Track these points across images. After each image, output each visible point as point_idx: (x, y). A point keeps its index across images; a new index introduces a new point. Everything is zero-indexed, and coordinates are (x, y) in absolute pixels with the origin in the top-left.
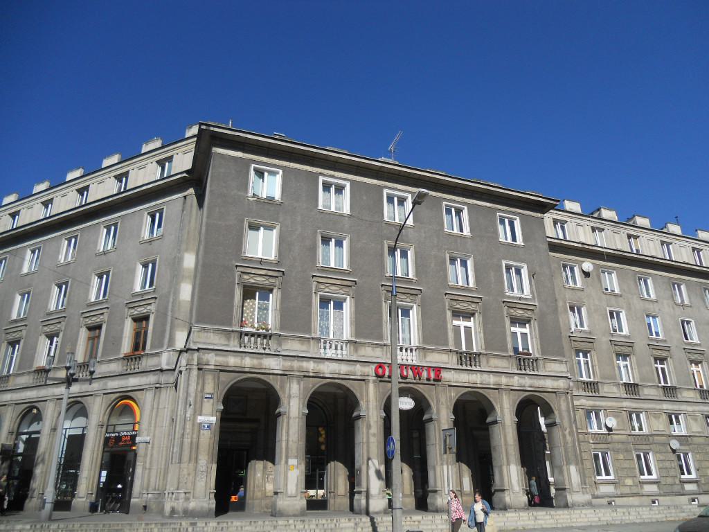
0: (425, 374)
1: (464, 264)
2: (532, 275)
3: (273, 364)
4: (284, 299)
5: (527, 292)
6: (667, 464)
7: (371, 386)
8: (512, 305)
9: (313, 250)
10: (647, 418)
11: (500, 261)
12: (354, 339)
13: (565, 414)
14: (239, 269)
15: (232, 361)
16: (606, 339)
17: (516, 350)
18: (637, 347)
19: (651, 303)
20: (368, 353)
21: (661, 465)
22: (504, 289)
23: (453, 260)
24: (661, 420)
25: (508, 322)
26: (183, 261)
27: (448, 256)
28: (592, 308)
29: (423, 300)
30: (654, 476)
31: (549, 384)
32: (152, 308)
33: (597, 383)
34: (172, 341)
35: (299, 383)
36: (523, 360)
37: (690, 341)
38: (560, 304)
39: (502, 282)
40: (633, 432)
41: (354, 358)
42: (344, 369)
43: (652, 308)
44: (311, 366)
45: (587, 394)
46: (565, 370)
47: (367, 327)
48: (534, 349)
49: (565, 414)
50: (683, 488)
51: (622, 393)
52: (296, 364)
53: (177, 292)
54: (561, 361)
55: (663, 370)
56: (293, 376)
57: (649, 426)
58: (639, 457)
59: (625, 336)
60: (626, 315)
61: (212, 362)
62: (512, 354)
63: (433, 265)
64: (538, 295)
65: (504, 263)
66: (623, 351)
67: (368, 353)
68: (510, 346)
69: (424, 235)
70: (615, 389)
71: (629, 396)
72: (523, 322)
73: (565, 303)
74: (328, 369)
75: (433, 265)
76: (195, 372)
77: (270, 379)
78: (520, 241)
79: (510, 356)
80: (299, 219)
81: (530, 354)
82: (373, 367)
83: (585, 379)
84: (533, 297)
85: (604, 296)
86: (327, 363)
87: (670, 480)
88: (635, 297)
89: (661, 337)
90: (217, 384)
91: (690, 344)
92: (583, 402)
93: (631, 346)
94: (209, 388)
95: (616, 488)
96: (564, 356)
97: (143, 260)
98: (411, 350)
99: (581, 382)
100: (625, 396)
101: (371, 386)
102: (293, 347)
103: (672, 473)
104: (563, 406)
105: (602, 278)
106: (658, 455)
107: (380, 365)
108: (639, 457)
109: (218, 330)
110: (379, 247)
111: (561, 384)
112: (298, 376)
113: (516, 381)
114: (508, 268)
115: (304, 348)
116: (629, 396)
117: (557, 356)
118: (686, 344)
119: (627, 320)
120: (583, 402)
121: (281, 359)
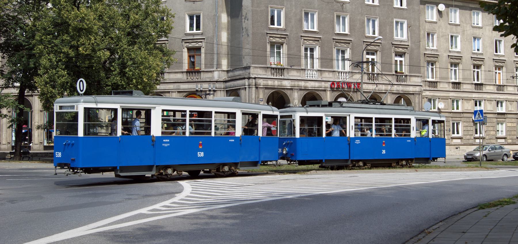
0: (353, 86)
1: (374, 22)
2: (409, 27)
3: (287, 84)
4: (289, 49)
5: (405, 37)
6: (469, 128)
7: (328, 93)
8: (397, 46)
9: (301, 21)
10: (462, 103)
11: (393, 19)
12: (320, 69)
13: (417, 105)
14: (268, 35)
15: (270, 83)
16: (446, 55)
17: (396, 72)
18: (464, 60)
19: (478, 29)
20: (328, 76)
21: (465, 129)
22: (393, 36)
23: (369, 20)
24: (470, 103)
25: (394, 55)
26: (221, 18)
27: (366, 18)
28: (441, 34)
29: (352, 46)
30: (460, 135)
31: (411, 89)
32: (203, 44)
33: (437, 82)
34: (219, 65)
35: (298, 93)
36: (399, 75)
37: (498, 53)
38: (422, 32)
39: (393, 33)
40: (453, 111)
41: (320, 79)
42: (317, 84)
43: (477, 32)
44: (302, 84)
45: (431, 89)
46: (420, 81)
47: (327, 62)
48: (405, 70)
49: (417, 105)
50: (475, 141)
51: (450, 87)
52: (296, 83)
53: (219, 37)
54: (418, 76)
55: (478, 72)
56: (295, 89)
57: (463, 107)
58: (453, 124)
59: (458, 52)
60: (461, 38)
61: (262, 84)
62: (394, 73)
63: (358, 25)
64: (411, 39)
65: (395, 20)
66: (455, 62)
67: (328, 76)
68: (394, 70)
69: (354, 7)
70: (446, 85)
71: (454, 90)
72: (401, 55)
73: (425, 32)
74: (310, 85)
75: (358, 25)
76: (254, 89)
77: (286, 92)
78: (404, 6)
79: (393, 75)
80: (294, 3)
81: (403, 73)
82: (330, 83)
83: (430, 79)
84: (408, 40)
85: (449, 26)
86: (309, 82)
87: (468, 137)
88: (468, 25)
89: (480, 52)
90: (264, 95)
91: (498, 56)
92: (427, 93)
93: (460, 58)
94: (261, 96)
95: (461, 141)
96: (420, 73)
97: (191, 13)
98: (346, 73)
99: (428, 81)
100: (452, 90)
101: (328, 93)
102: (294, 74)
103: (470, 133)
104: (417, 100)
105: (450, 13)
106: (465, 123)
107: (333, 83)
108: (453, 124)
109: (262, 67)
110: (332, 16)
111: (417, 89)
112: (297, 89)
113: (395, 88)
114: (397, 23)
115: (298, 74)
116: (454, 90)
117: (417, 73)
118: (495, 55)
119: (461, 41)
120: (427, 93)
121: (290, 81)
